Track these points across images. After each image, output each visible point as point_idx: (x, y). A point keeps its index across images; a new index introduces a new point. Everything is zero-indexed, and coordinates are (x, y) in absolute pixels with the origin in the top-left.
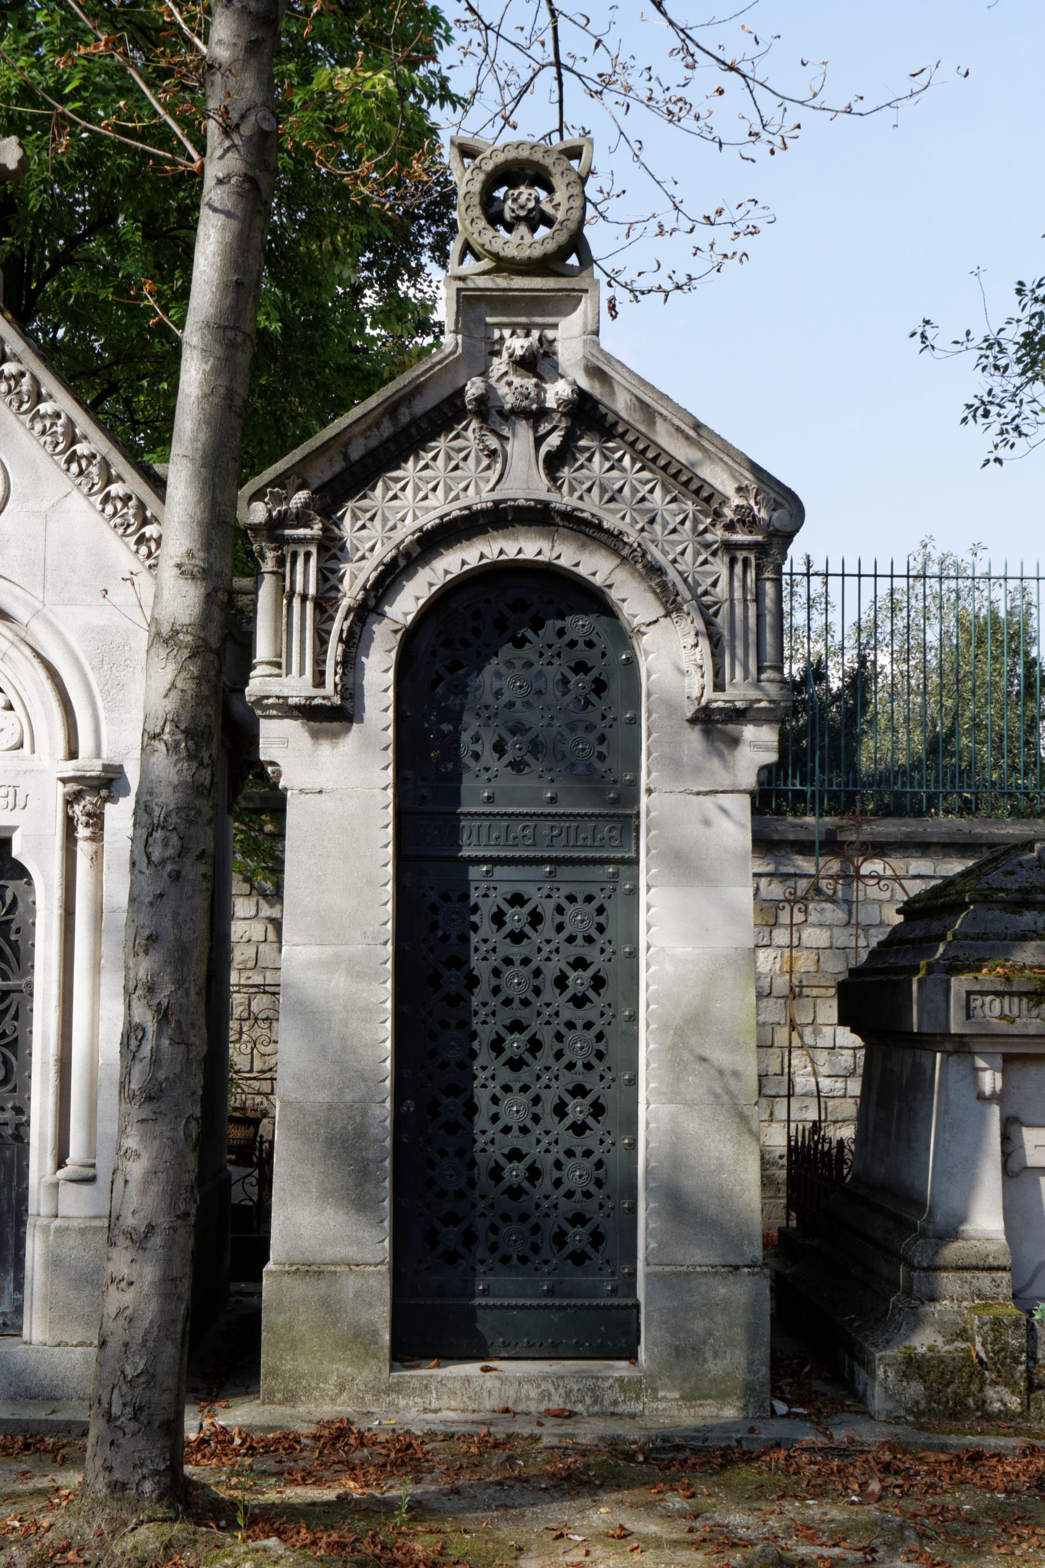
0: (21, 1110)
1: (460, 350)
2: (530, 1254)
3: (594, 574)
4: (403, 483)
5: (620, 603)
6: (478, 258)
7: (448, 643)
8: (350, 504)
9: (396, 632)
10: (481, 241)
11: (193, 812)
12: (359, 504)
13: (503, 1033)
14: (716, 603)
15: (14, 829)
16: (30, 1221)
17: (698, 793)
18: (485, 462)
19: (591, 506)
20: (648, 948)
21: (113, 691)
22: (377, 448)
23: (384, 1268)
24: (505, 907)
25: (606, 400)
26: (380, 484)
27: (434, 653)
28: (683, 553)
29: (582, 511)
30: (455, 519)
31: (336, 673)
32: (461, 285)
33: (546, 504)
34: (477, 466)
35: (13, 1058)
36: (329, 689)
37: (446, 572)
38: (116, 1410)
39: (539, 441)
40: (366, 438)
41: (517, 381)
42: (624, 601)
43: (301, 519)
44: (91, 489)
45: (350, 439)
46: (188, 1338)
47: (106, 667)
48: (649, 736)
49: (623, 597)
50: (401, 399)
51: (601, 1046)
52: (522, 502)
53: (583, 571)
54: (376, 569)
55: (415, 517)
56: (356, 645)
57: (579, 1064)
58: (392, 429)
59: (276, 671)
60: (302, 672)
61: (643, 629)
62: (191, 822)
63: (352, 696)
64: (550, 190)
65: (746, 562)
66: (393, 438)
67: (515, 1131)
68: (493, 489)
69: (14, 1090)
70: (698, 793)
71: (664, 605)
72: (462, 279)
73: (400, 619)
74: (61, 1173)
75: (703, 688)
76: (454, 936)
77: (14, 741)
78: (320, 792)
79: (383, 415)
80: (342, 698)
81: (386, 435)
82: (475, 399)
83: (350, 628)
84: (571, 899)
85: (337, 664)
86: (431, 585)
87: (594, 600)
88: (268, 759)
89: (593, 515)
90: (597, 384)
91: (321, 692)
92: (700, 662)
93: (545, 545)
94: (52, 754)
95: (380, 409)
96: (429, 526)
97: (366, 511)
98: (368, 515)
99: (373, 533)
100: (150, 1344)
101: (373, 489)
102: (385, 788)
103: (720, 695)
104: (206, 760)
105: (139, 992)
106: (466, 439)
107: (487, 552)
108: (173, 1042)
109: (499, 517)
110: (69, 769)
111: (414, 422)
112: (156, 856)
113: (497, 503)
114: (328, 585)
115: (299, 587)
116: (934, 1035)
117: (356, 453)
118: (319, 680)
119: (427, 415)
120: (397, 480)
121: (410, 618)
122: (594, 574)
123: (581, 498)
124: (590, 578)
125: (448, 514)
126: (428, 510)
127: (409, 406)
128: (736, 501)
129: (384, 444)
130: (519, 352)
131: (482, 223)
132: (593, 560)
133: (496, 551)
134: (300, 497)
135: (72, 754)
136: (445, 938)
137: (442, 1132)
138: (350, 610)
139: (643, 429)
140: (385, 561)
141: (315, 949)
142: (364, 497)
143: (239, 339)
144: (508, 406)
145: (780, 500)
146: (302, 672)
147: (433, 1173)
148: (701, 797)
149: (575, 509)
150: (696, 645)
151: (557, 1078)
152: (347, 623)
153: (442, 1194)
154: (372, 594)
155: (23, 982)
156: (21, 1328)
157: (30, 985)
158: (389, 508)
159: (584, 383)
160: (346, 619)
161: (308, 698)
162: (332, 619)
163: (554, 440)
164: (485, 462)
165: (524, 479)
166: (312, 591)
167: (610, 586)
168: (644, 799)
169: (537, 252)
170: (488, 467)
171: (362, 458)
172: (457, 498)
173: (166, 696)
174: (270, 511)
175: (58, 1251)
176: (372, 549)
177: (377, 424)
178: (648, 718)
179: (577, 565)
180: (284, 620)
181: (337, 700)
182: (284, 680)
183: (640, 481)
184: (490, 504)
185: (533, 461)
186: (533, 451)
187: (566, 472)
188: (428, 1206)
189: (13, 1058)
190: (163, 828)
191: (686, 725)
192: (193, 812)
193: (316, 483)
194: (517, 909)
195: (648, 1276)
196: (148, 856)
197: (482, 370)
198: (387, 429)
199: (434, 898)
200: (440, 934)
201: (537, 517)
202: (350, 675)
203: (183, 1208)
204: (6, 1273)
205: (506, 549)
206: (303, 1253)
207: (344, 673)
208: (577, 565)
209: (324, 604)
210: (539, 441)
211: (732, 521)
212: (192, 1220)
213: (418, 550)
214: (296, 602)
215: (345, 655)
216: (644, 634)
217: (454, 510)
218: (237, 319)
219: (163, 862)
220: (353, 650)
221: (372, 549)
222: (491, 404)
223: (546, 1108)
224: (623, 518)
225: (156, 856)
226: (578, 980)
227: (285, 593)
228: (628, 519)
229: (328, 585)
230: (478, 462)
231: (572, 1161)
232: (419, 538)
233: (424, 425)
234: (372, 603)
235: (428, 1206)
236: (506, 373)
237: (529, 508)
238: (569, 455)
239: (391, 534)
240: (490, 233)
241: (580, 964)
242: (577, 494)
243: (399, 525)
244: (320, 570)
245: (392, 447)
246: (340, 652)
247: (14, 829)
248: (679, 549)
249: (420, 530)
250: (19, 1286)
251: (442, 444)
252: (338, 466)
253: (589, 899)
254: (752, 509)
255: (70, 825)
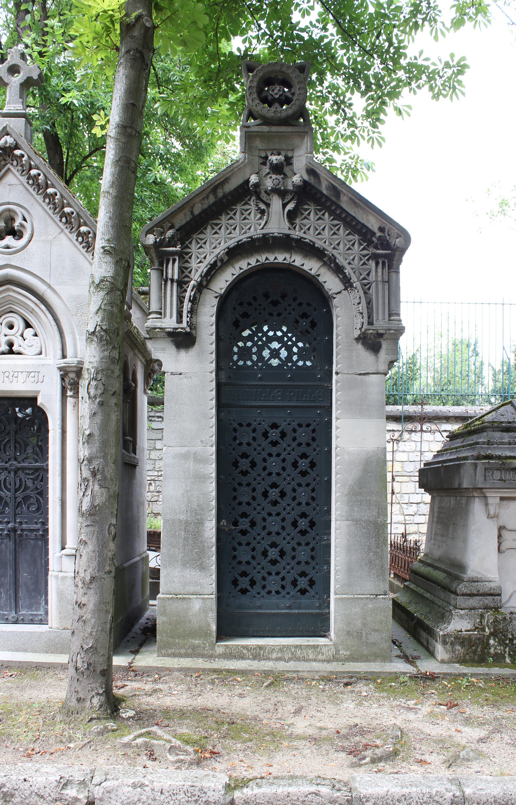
0: (45, 523)
1: (247, 161)
2: (281, 590)
3: (311, 270)
4: (219, 226)
5: (323, 284)
6: (255, 119)
7: (241, 304)
8: (195, 236)
9: (216, 297)
10: (256, 109)
11: (110, 372)
12: (198, 236)
13: (268, 488)
14: (369, 283)
15: (38, 392)
16: (50, 573)
17: (360, 374)
18: (259, 216)
19: (310, 237)
20: (336, 448)
21: (82, 326)
22: (207, 209)
23: (213, 596)
24: (269, 429)
25: (317, 186)
26: (209, 227)
27: (234, 309)
28: (353, 260)
29: (305, 239)
30: (244, 242)
31: (188, 317)
32: (246, 130)
33: (288, 236)
34: (255, 218)
35: (41, 499)
36: (184, 324)
37: (241, 269)
38: (79, 665)
39: (284, 206)
40: (202, 204)
41: (274, 176)
42: (325, 282)
43: (171, 243)
44: (71, 230)
45: (194, 204)
46: (113, 630)
47: (79, 315)
48: (337, 347)
49: (325, 280)
50: (219, 184)
51: (314, 494)
52: (276, 234)
53: (306, 268)
54: (206, 267)
55: (226, 242)
56: (197, 304)
57: (304, 503)
58: (214, 200)
59: (159, 316)
60: (171, 317)
61: (334, 296)
62: (108, 377)
63: (195, 328)
64: (290, 87)
65: (384, 264)
66: (214, 204)
67: (304, 445)
68: (262, 228)
69: (42, 514)
70: (360, 374)
71: (344, 284)
72: (249, 127)
73: (219, 291)
74: (64, 552)
75: (363, 324)
76: (245, 443)
77: (38, 351)
78: (180, 374)
79: (210, 193)
80: (191, 329)
81: (211, 202)
82: (253, 185)
83: (194, 295)
84: (300, 425)
85: (188, 312)
86: (233, 275)
87: (312, 283)
88: (155, 358)
89: (310, 241)
90: (312, 178)
91: (181, 326)
92: (361, 311)
93: (288, 256)
94: (55, 357)
95: (209, 190)
96: (232, 246)
97: (202, 239)
98: (203, 241)
99: (205, 250)
100: (94, 633)
101: (205, 229)
102: (211, 372)
103: (370, 327)
104: (116, 344)
105: (85, 462)
106: (250, 205)
107: (260, 259)
108: (101, 486)
109: (266, 243)
110: (62, 363)
111: (225, 196)
112: (92, 394)
113: (264, 235)
114: (184, 275)
115: (170, 276)
116: (469, 489)
117: (197, 211)
118: (180, 320)
119: (231, 193)
120: (217, 225)
121: (223, 291)
122: (311, 270)
123: (305, 233)
124: (309, 271)
125: (241, 240)
126: (231, 239)
127: (222, 188)
128: (378, 234)
129: (210, 207)
130: (275, 162)
131: (257, 101)
132: (310, 263)
133: (264, 258)
134: (170, 233)
135: (64, 356)
136: (240, 444)
137: (239, 534)
138: (194, 286)
139: (334, 199)
140: (211, 262)
141: (179, 449)
142: (202, 232)
143: (133, 133)
144: (270, 188)
145: (399, 233)
146: (171, 317)
147: (235, 553)
148: (362, 376)
149: (301, 238)
150: (359, 303)
151: (293, 509)
152: (193, 293)
153: (240, 563)
154: (205, 279)
155: (45, 464)
156: (47, 621)
157: (47, 465)
158: (213, 238)
159: (306, 177)
160: (192, 291)
161: (174, 329)
162: (186, 291)
163: (290, 206)
164: (259, 216)
165: (277, 224)
166: (176, 277)
167: (319, 275)
168: (334, 377)
169: (284, 114)
170: (261, 218)
171: (200, 214)
172: (245, 233)
173: (97, 313)
174: (156, 239)
175: (62, 587)
176: (205, 258)
177: (207, 197)
178: (337, 338)
179: (303, 265)
180: (163, 291)
181: (188, 330)
182: (163, 320)
183: (333, 225)
184: (261, 235)
185: (282, 215)
186: (281, 210)
187: (297, 221)
188: (233, 568)
189: (41, 499)
190: (96, 380)
191: (355, 341)
192: (110, 372)
193: (177, 226)
194: (274, 430)
195: (336, 599)
196: (89, 393)
197: (257, 171)
198: (212, 199)
199: (236, 425)
200: (238, 442)
201: (285, 243)
202: (194, 318)
203: (108, 568)
204: (42, 597)
205: (269, 258)
206: (175, 589)
207: (191, 317)
208: (303, 265)
209: (182, 284)
210: (284, 206)
211: (377, 244)
212: (113, 574)
213: (227, 258)
214: (169, 282)
215: (192, 308)
216: (335, 298)
217: (244, 238)
218: (132, 123)
219: (95, 397)
220: (196, 306)
221: (205, 258)
222: (261, 187)
223: (274, 538)
224: (325, 242)
225: (92, 394)
226: (303, 464)
227: (164, 280)
228: (327, 243)
229: (184, 275)
230: (255, 216)
231: (300, 548)
232: (227, 252)
233: (230, 198)
234: (204, 283)
235: (233, 568)
236: (269, 173)
237: (280, 237)
238: (299, 212)
239: (214, 250)
240: (262, 105)
241: (304, 456)
242: (303, 231)
243: (218, 246)
244: (180, 268)
245: (214, 208)
246: (189, 307)
247: (38, 392)
248: (351, 257)
249: (228, 248)
250: (47, 603)
251: (239, 207)
252: (189, 217)
253: (308, 425)
254: (386, 237)
255: (64, 390)
